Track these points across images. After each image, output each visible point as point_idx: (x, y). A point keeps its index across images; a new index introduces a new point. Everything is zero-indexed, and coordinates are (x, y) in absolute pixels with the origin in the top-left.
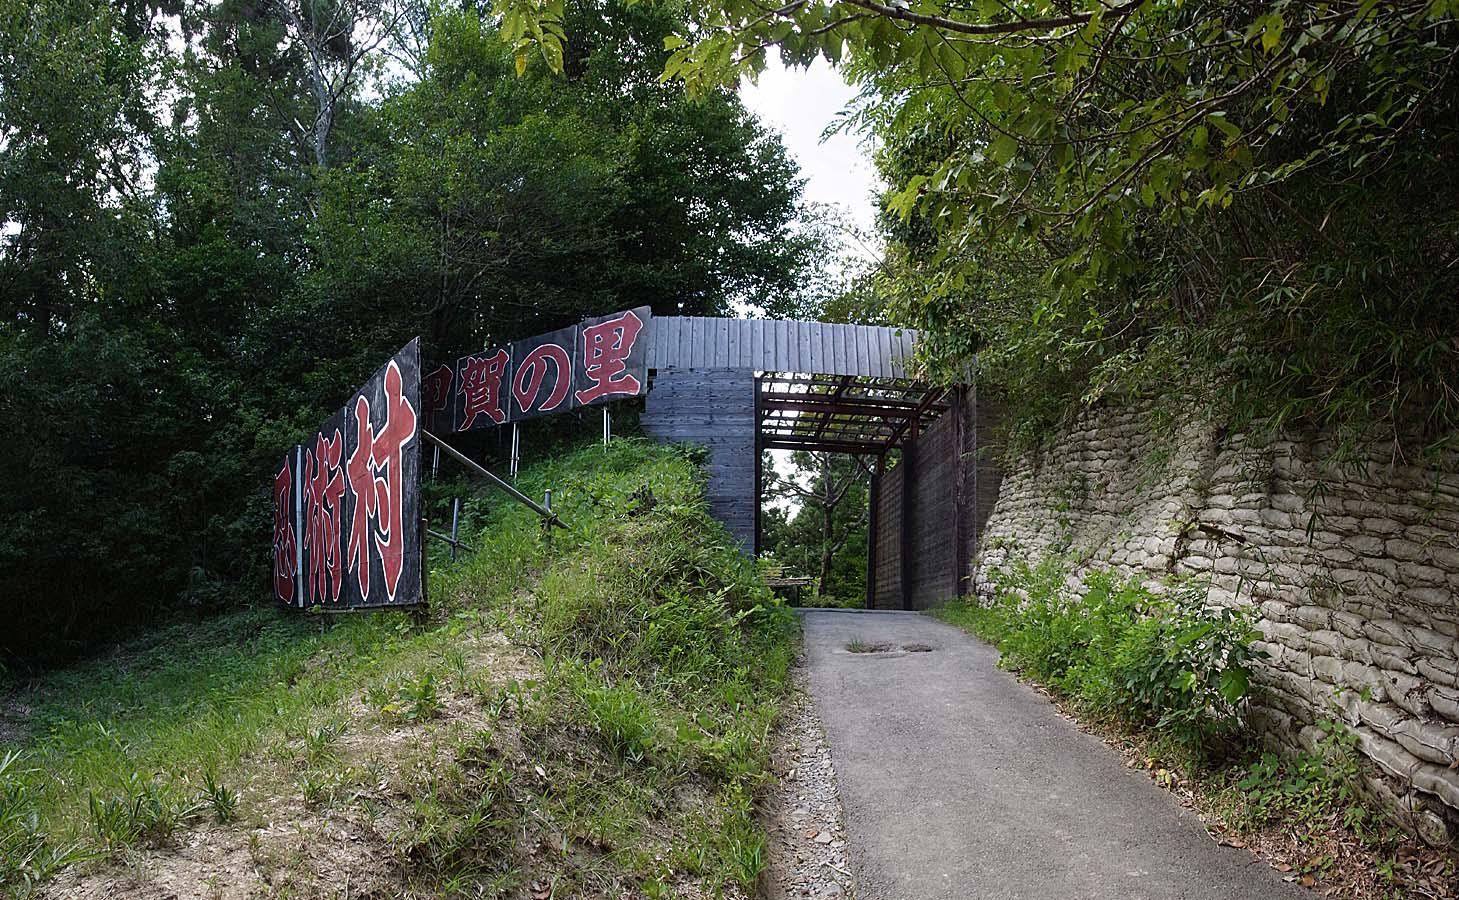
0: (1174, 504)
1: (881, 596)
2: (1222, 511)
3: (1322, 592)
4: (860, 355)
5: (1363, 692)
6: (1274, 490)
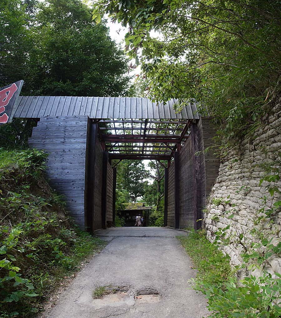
4: (143, 109)
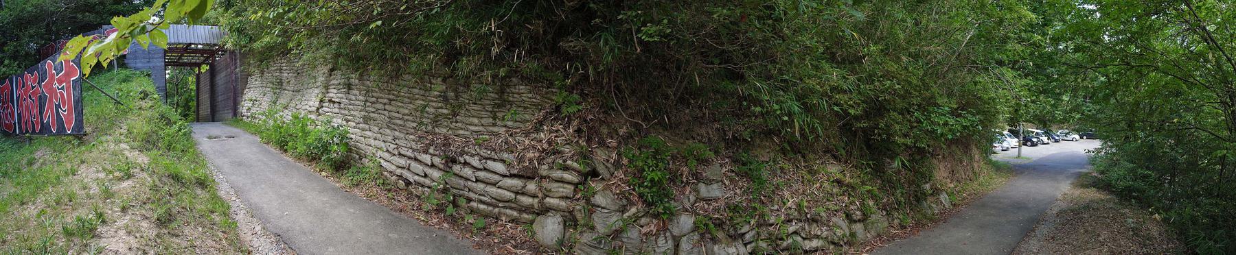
0: (317, 91)
1: (568, 176)
2: (333, 94)
3: (366, 120)
5: (381, 149)
6: (349, 88)
